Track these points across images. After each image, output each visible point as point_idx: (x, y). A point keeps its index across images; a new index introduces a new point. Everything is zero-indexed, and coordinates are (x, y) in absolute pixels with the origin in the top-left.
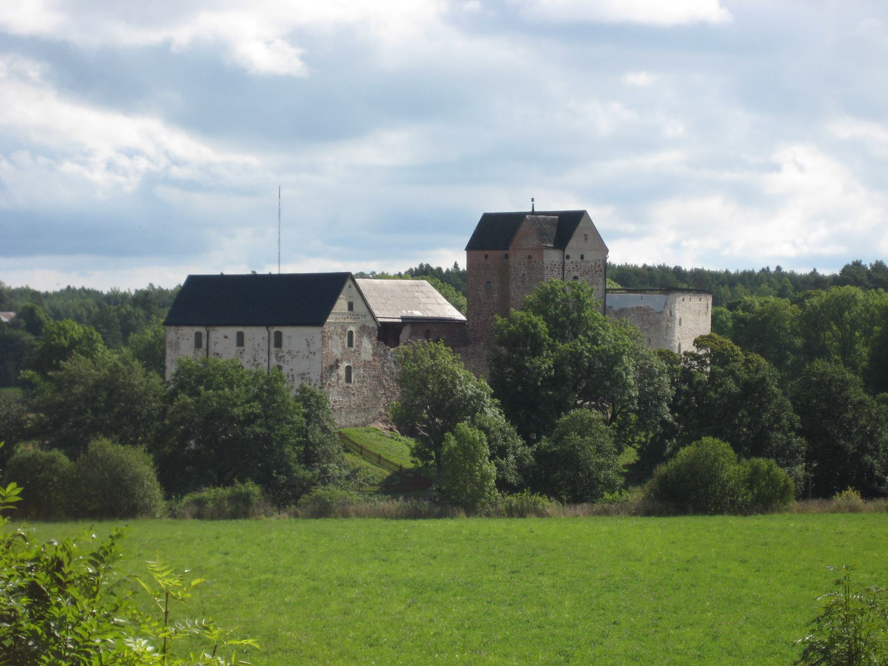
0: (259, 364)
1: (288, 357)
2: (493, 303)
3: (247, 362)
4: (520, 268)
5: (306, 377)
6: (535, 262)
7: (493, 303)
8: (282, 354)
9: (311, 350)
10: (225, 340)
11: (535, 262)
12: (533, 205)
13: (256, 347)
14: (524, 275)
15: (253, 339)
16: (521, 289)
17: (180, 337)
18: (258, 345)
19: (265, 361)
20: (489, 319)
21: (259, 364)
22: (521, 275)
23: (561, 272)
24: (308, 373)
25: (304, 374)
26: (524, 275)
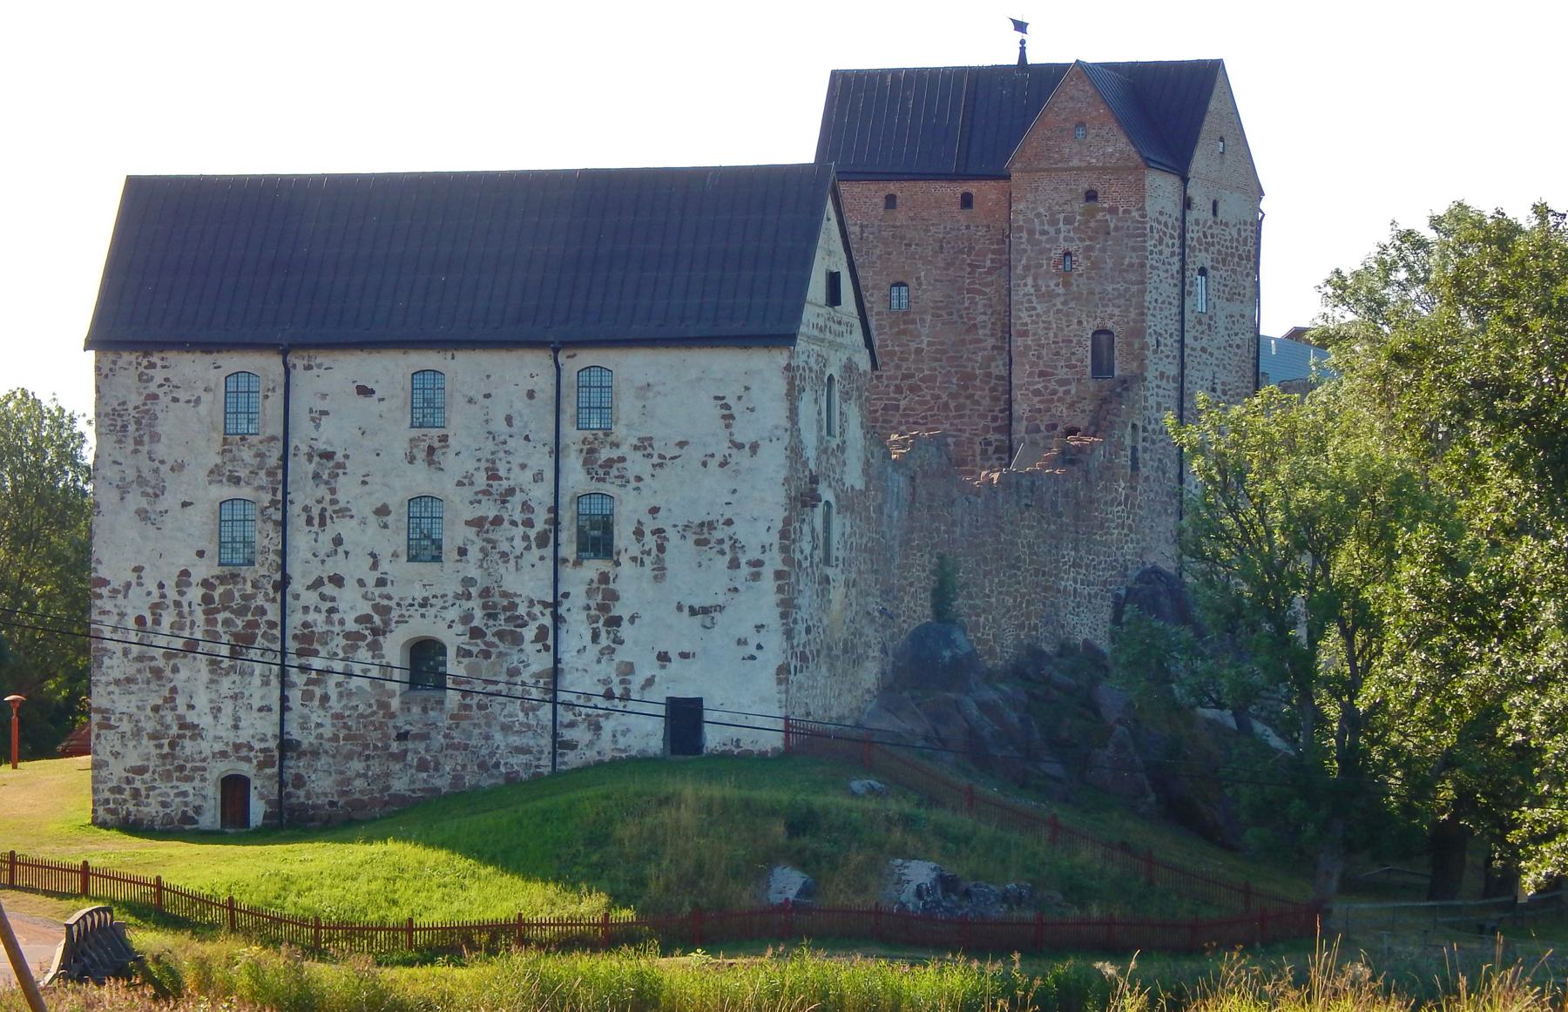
0: (511, 491)
1: (637, 464)
2: (919, 351)
3: (460, 484)
4: (1052, 230)
5: (718, 535)
6: (1113, 210)
7: (919, 351)
8: (615, 454)
9: (738, 438)
10: (363, 401)
11: (1113, 210)
12: (1023, 42)
13: (500, 426)
14: (1067, 254)
15: (487, 396)
16: (1058, 302)
17: (160, 392)
18: (509, 420)
19: (538, 477)
20: (903, 404)
21: (511, 491)
22: (1056, 254)
23: (1177, 250)
24: (729, 522)
25: (711, 526)
26: (1067, 254)
